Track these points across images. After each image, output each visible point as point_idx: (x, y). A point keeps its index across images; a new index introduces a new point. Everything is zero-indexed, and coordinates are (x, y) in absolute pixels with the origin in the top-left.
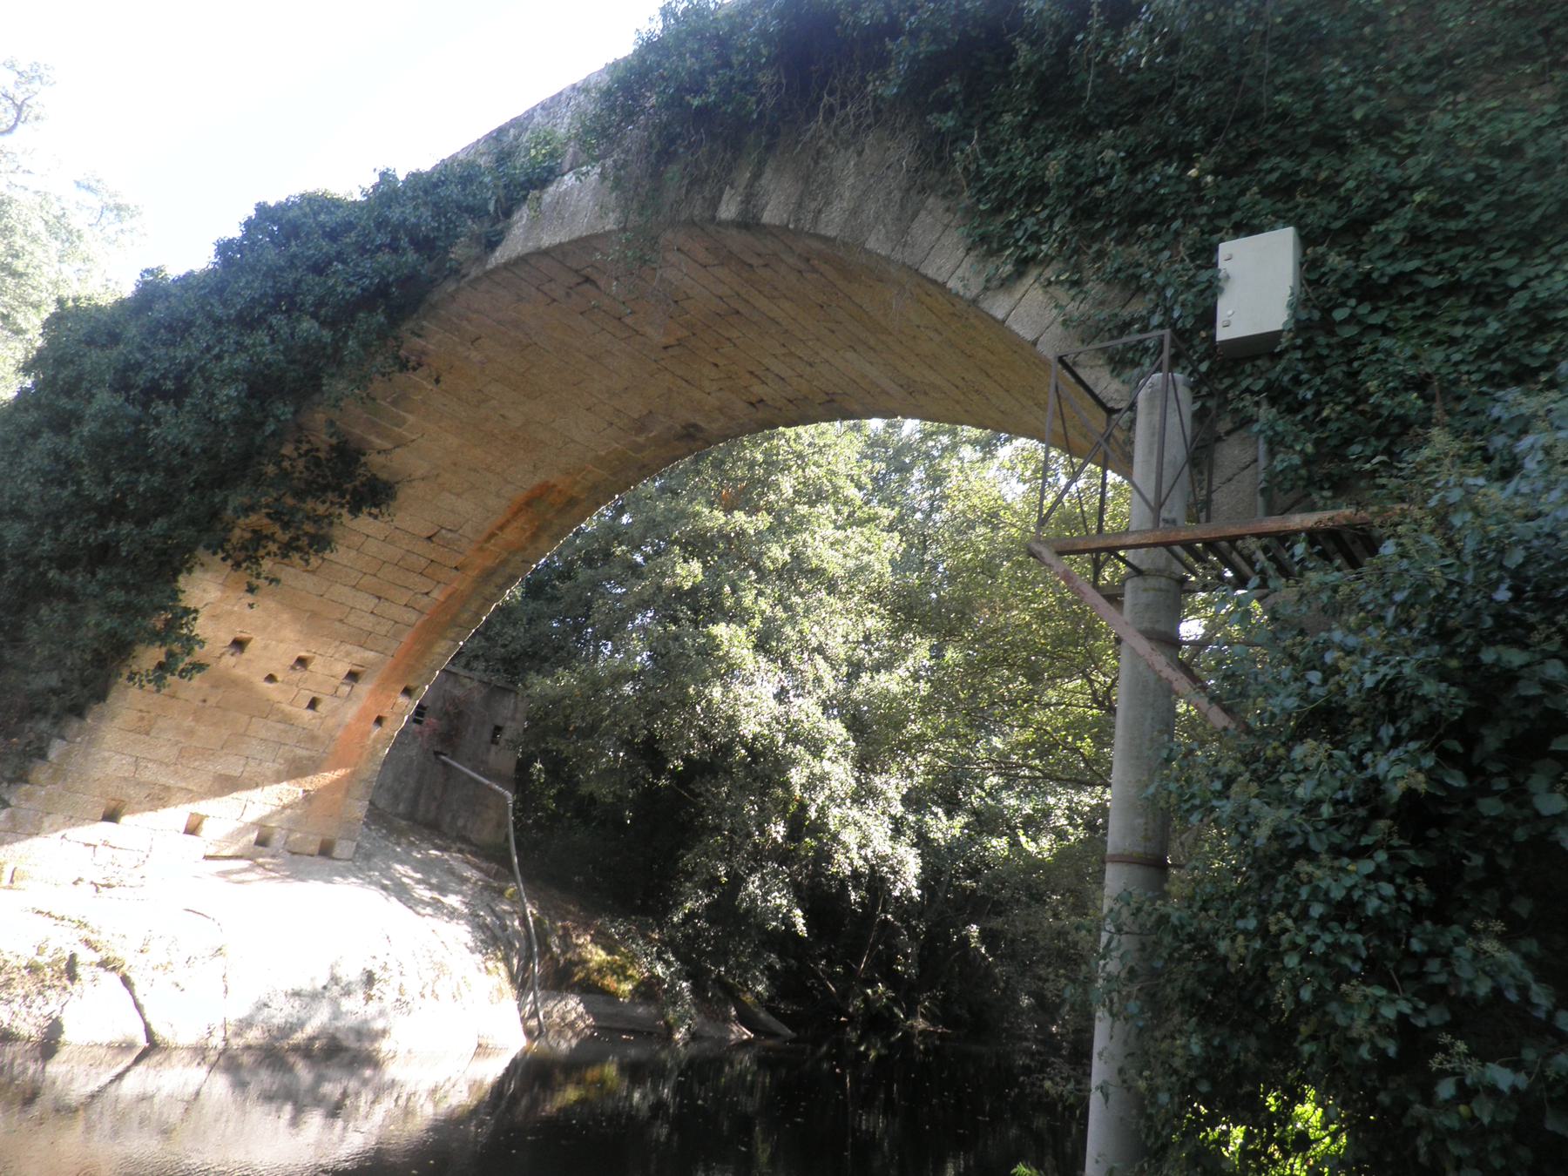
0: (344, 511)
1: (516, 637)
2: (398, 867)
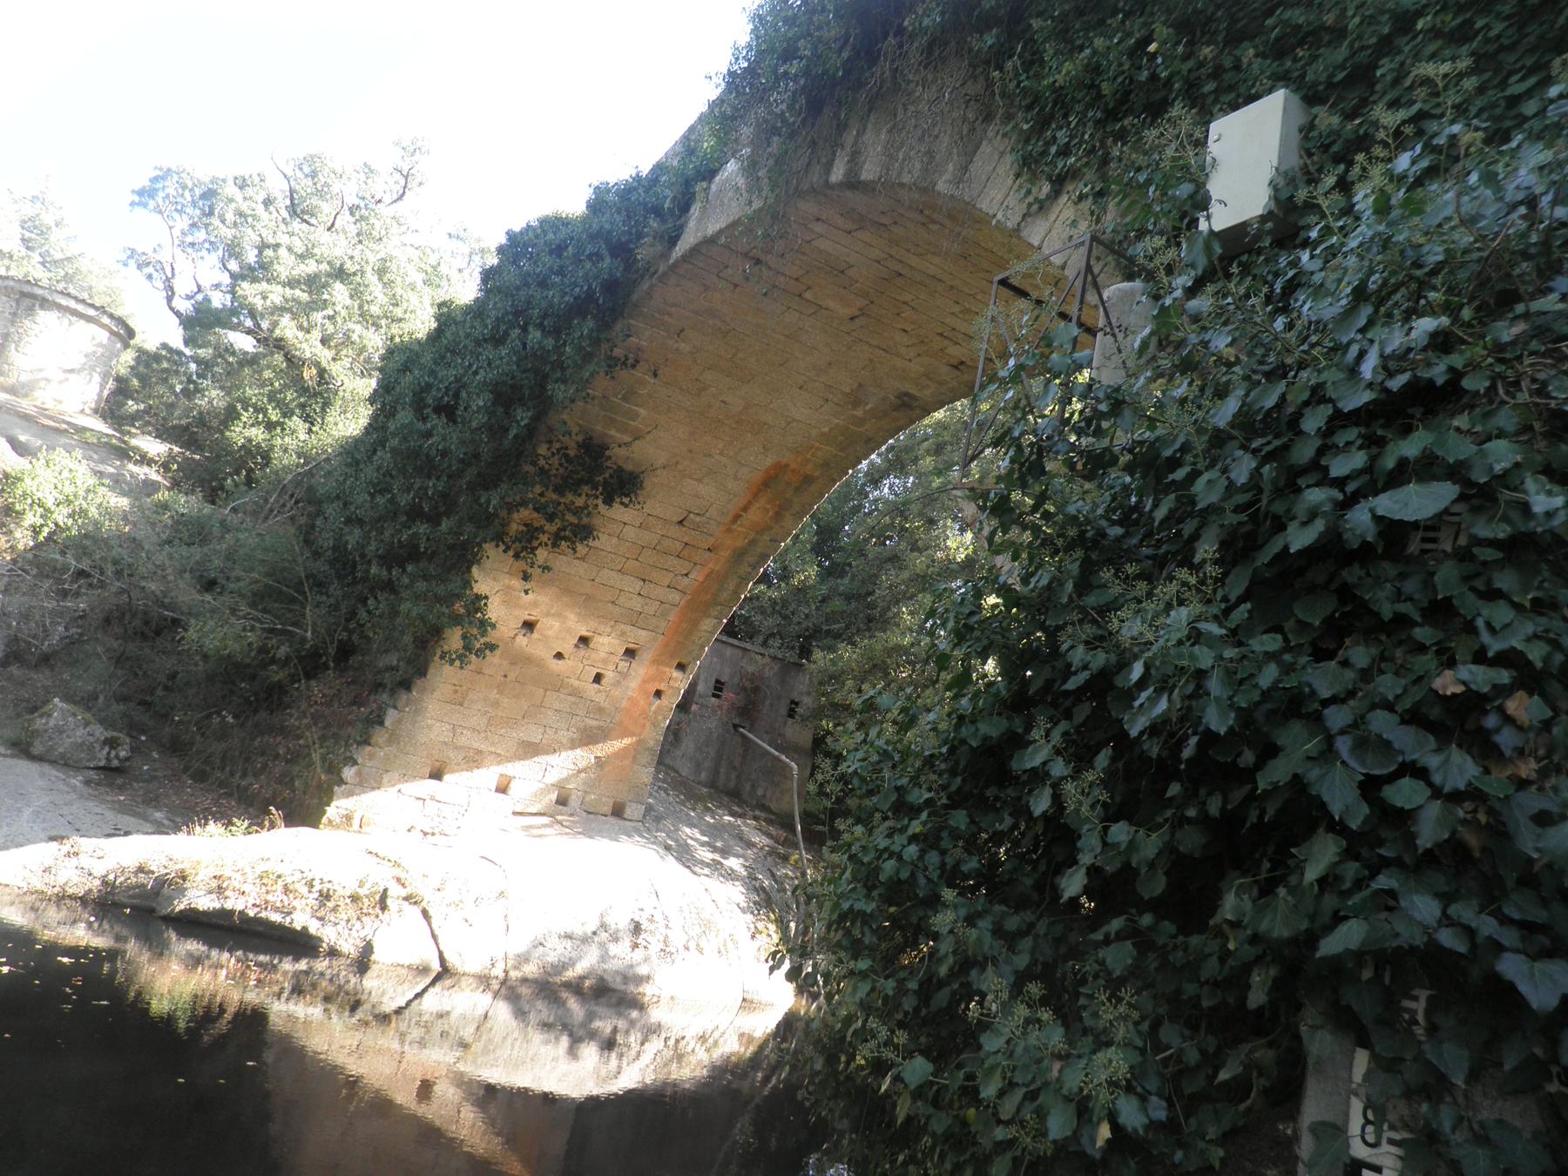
0: (599, 502)
2: (687, 830)
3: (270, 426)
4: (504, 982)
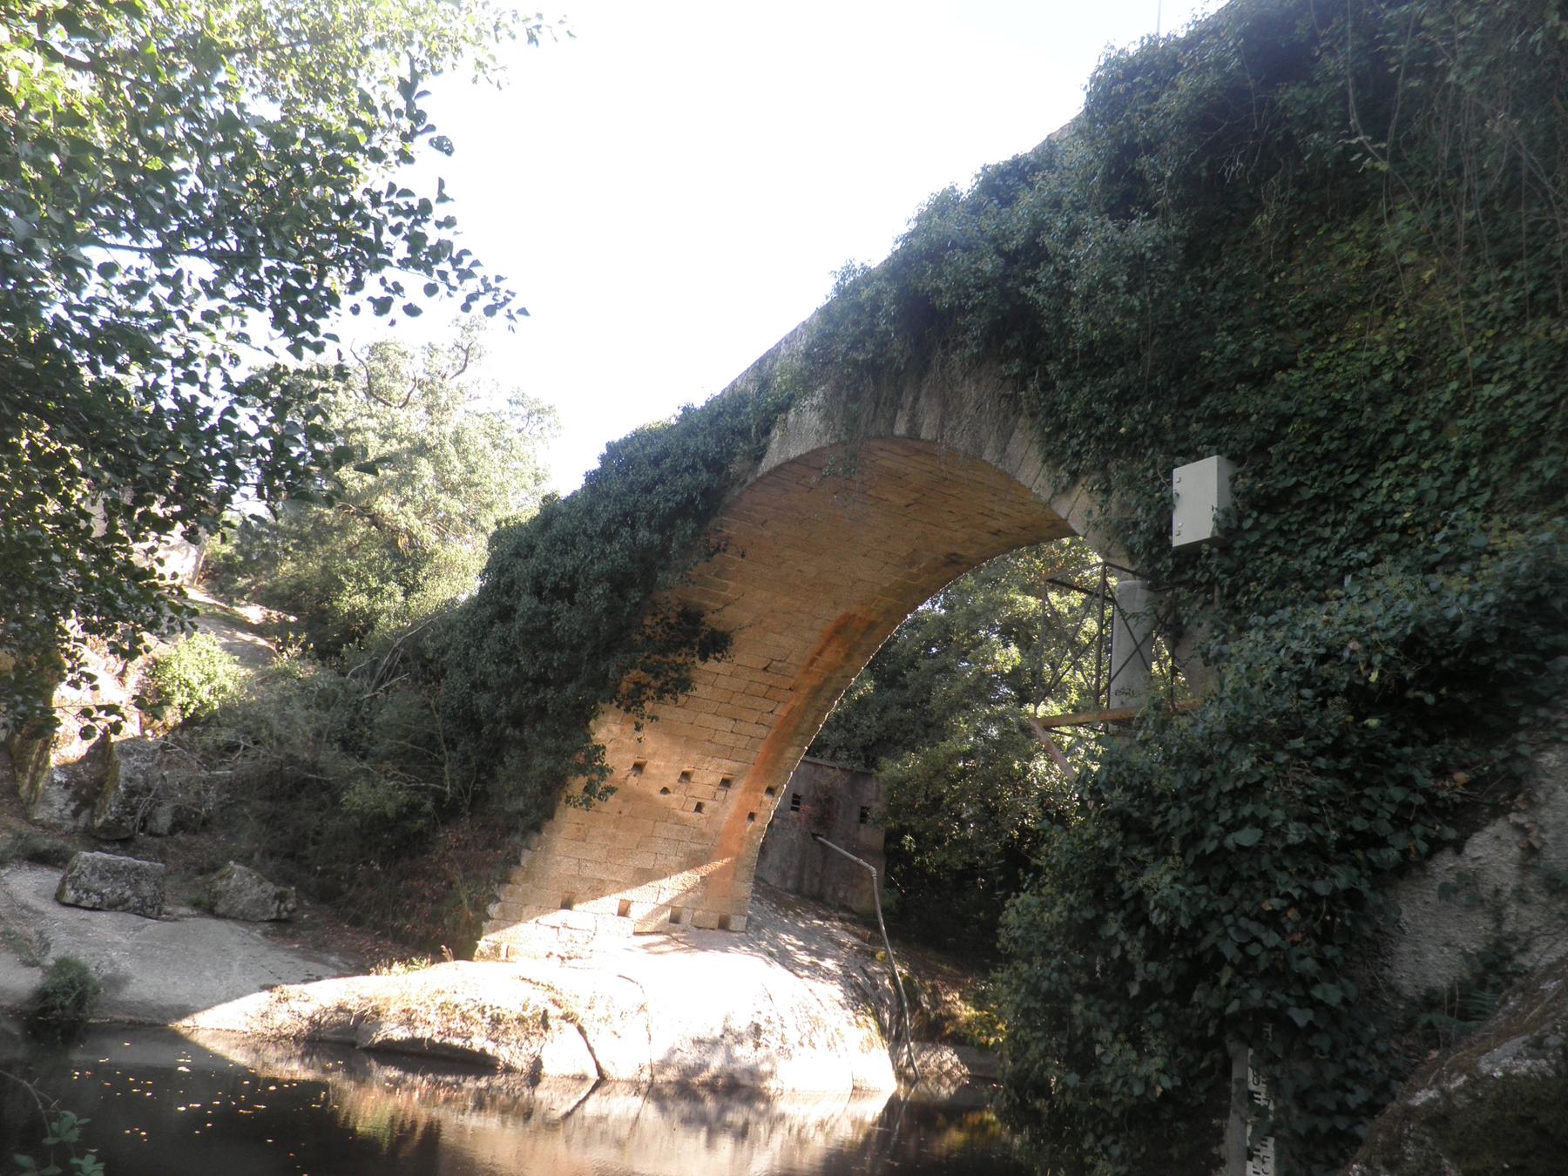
0: (697, 659)
1: (870, 725)
3: (372, 593)
4: (651, 1085)
